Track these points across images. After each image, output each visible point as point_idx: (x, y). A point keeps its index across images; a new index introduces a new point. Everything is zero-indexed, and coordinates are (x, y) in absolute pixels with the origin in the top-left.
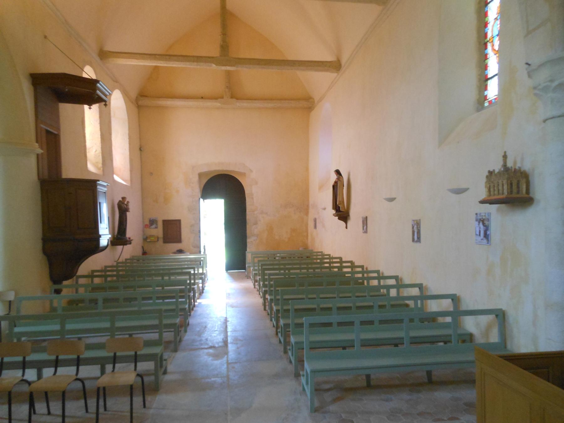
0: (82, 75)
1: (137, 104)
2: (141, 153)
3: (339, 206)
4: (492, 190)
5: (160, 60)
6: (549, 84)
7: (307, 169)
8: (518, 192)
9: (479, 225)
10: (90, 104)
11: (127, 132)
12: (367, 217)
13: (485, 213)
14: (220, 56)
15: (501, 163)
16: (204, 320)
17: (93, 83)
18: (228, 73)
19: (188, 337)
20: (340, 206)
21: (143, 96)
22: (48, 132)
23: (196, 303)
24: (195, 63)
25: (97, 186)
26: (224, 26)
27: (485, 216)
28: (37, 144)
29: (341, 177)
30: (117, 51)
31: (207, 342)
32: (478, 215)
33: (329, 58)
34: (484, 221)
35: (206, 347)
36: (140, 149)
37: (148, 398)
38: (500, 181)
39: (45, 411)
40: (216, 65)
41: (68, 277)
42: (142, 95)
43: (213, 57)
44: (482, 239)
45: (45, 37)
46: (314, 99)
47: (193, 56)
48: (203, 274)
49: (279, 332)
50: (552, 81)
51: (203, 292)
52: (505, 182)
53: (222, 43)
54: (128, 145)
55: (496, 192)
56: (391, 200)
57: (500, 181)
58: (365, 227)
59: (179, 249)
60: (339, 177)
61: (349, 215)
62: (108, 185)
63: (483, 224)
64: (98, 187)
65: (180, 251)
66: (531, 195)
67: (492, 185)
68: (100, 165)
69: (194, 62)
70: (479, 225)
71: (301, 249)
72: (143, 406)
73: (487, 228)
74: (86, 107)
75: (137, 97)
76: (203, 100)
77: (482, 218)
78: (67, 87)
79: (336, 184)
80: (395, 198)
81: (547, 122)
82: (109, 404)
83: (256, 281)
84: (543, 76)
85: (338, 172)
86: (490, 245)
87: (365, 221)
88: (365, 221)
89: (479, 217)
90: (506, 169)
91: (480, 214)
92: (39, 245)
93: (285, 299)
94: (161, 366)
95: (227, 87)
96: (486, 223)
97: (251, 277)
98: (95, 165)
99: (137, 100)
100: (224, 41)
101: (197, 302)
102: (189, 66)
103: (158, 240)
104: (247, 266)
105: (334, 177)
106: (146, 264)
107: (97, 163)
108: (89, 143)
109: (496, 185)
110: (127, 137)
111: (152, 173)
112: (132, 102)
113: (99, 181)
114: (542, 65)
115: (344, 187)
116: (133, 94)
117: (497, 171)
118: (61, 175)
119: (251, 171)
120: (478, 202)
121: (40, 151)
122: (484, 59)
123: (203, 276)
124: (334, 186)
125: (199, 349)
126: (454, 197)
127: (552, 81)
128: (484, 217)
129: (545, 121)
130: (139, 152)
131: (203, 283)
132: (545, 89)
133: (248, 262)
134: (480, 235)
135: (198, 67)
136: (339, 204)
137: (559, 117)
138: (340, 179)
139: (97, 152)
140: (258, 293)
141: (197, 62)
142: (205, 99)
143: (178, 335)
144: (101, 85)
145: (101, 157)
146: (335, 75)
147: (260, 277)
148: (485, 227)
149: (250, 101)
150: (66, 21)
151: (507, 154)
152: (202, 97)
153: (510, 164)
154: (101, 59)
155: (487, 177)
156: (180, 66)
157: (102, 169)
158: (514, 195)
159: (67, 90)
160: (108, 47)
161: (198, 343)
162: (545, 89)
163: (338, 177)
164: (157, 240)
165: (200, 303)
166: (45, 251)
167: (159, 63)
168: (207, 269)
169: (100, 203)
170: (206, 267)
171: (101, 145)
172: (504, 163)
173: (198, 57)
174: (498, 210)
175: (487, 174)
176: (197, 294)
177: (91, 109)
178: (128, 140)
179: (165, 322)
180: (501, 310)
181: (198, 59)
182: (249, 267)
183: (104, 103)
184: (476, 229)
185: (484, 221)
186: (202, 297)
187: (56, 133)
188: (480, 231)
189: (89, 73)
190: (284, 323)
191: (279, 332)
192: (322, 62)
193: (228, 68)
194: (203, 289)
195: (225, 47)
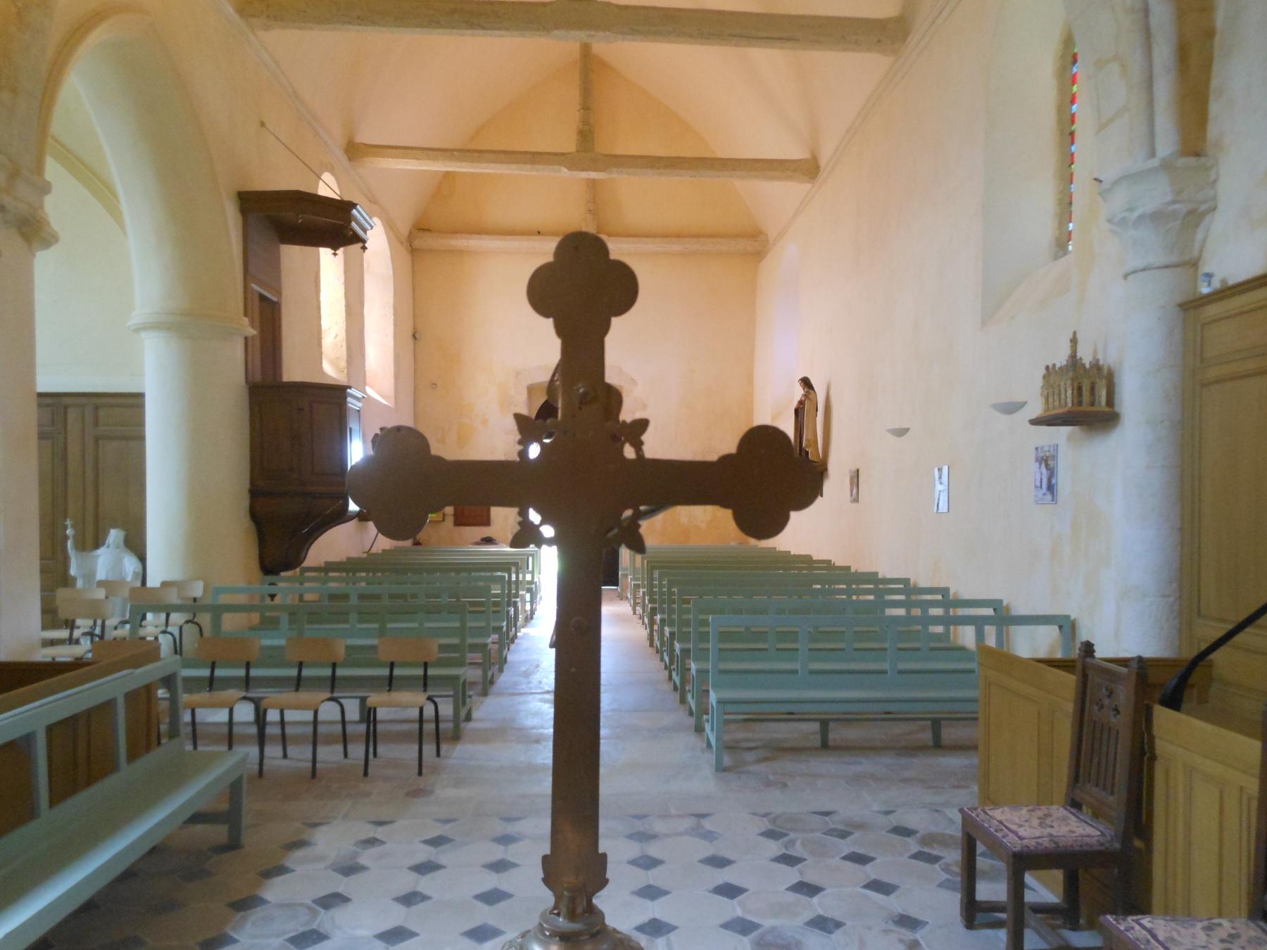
0: (317, 190)
1: (410, 246)
2: (415, 344)
3: (807, 450)
4: (1051, 400)
5: (458, 159)
6: (1126, 214)
7: (750, 380)
8: (1092, 404)
9: (1040, 468)
10: (335, 247)
11: (392, 301)
12: (858, 471)
13: (1050, 446)
14: (577, 151)
15: (1068, 352)
16: (535, 656)
17: (343, 208)
18: (592, 184)
19: (504, 679)
20: (809, 450)
21: (421, 229)
22: (262, 298)
23: (518, 634)
24: (529, 166)
25: (346, 398)
26: (587, 91)
27: (1049, 451)
28: (246, 319)
29: (812, 392)
30: (372, 143)
31: (541, 685)
32: (1039, 451)
33: (795, 152)
34: (1047, 461)
35: (539, 691)
36: (414, 336)
37: (444, 747)
38: (1062, 384)
39: (279, 752)
40: (570, 169)
41: (289, 566)
42: (421, 228)
43: (563, 154)
44: (1044, 495)
45: (262, 124)
46: (767, 235)
47: (526, 153)
48: (532, 582)
49: (674, 669)
50: (1130, 210)
51: (532, 618)
52: (1069, 382)
53: (581, 126)
54: (392, 327)
55: (1057, 403)
56: (901, 432)
57: (1062, 384)
58: (855, 491)
59: (486, 536)
60: (808, 392)
61: (826, 469)
62: (363, 397)
63: (1047, 466)
64: (349, 399)
65: (488, 541)
66: (1117, 409)
67: (1051, 390)
68: (343, 364)
69: (525, 163)
70: (1040, 468)
71: (732, 544)
72: (435, 755)
73: (1052, 473)
74: (325, 253)
75: (410, 233)
76: (539, 237)
77: (1045, 456)
78: (300, 216)
79: (801, 406)
80: (908, 430)
81: (1130, 278)
82: (380, 749)
83: (635, 605)
84: (1120, 199)
85: (806, 382)
86: (1056, 503)
87: (856, 477)
88: (856, 477)
89: (1041, 454)
90: (1074, 361)
91: (1042, 448)
92: (245, 502)
93: (700, 649)
94: (464, 703)
95: (590, 211)
96: (1051, 463)
97: (629, 595)
98: (334, 363)
99: (411, 238)
100: (585, 121)
101: (520, 632)
102: (516, 172)
103: (443, 520)
104: (620, 573)
105: (799, 392)
106: (409, 586)
107: (338, 358)
108: (326, 322)
109: (1057, 391)
110: (391, 311)
111: (435, 384)
112: (402, 243)
113: (350, 388)
114: (1116, 183)
115: (818, 413)
116: (404, 227)
117: (1058, 366)
118: (281, 376)
119: (634, 382)
120: (1028, 424)
121: (252, 332)
122: (1070, 163)
123: (533, 586)
124: (796, 411)
125: (525, 693)
126: (1004, 418)
127: (1130, 210)
128: (1048, 454)
129: (1126, 276)
130: (411, 340)
131: (532, 602)
132: (1123, 222)
133: (624, 566)
134: (1041, 488)
135: (534, 173)
136: (807, 446)
137: (1144, 270)
138: (811, 397)
139: (338, 339)
140: (641, 621)
141: (533, 163)
142: (544, 235)
143: (490, 669)
144: (359, 212)
145: (344, 348)
146: (808, 186)
147: (645, 590)
148: (1049, 472)
149: (635, 239)
150: (294, 92)
151: (1078, 336)
152: (539, 232)
153: (1086, 356)
154: (350, 160)
155: (1044, 377)
156: (499, 172)
157: (346, 370)
158: (1086, 407)
159: (300, 221)
160: (366, 136)
161: (524, 686)
162: (1123, 222)
163: (806, 392)
164: (441, 520)
165: (524, 634)
166: (254, 515)
167: (459, 167)
168: (540, 576)
169: (351, 429)
170: (540, 573)
171: (346, 325)
172: (1072, 353)
173: (534, 154)
174: (1070, 438)
175: (1043, 371)
176: (520, 616)
177: (337, 256)
178: (393, 317)
179: (470, 641)
180: (1067, 617)
181: (535, 158)
182: (626, 576)
183: (360, 245)
184: (1035, 476)
185: (1047, 461)
186: (529, 625)
187: (275, 299)
188: (1041, 479)
189: (328, 188)
190: (682, 646)
191: (674, 669)
192: (782, 163)
193: (593, 175)
194: (533, 612)
195: (586, 135)
